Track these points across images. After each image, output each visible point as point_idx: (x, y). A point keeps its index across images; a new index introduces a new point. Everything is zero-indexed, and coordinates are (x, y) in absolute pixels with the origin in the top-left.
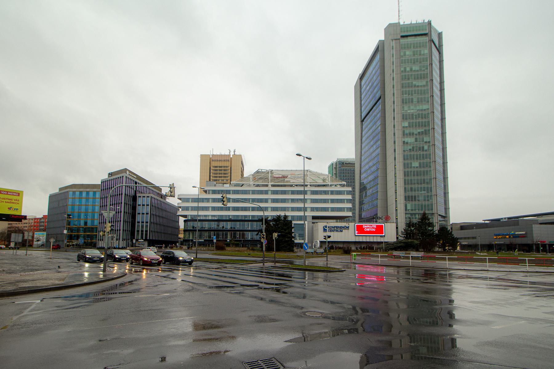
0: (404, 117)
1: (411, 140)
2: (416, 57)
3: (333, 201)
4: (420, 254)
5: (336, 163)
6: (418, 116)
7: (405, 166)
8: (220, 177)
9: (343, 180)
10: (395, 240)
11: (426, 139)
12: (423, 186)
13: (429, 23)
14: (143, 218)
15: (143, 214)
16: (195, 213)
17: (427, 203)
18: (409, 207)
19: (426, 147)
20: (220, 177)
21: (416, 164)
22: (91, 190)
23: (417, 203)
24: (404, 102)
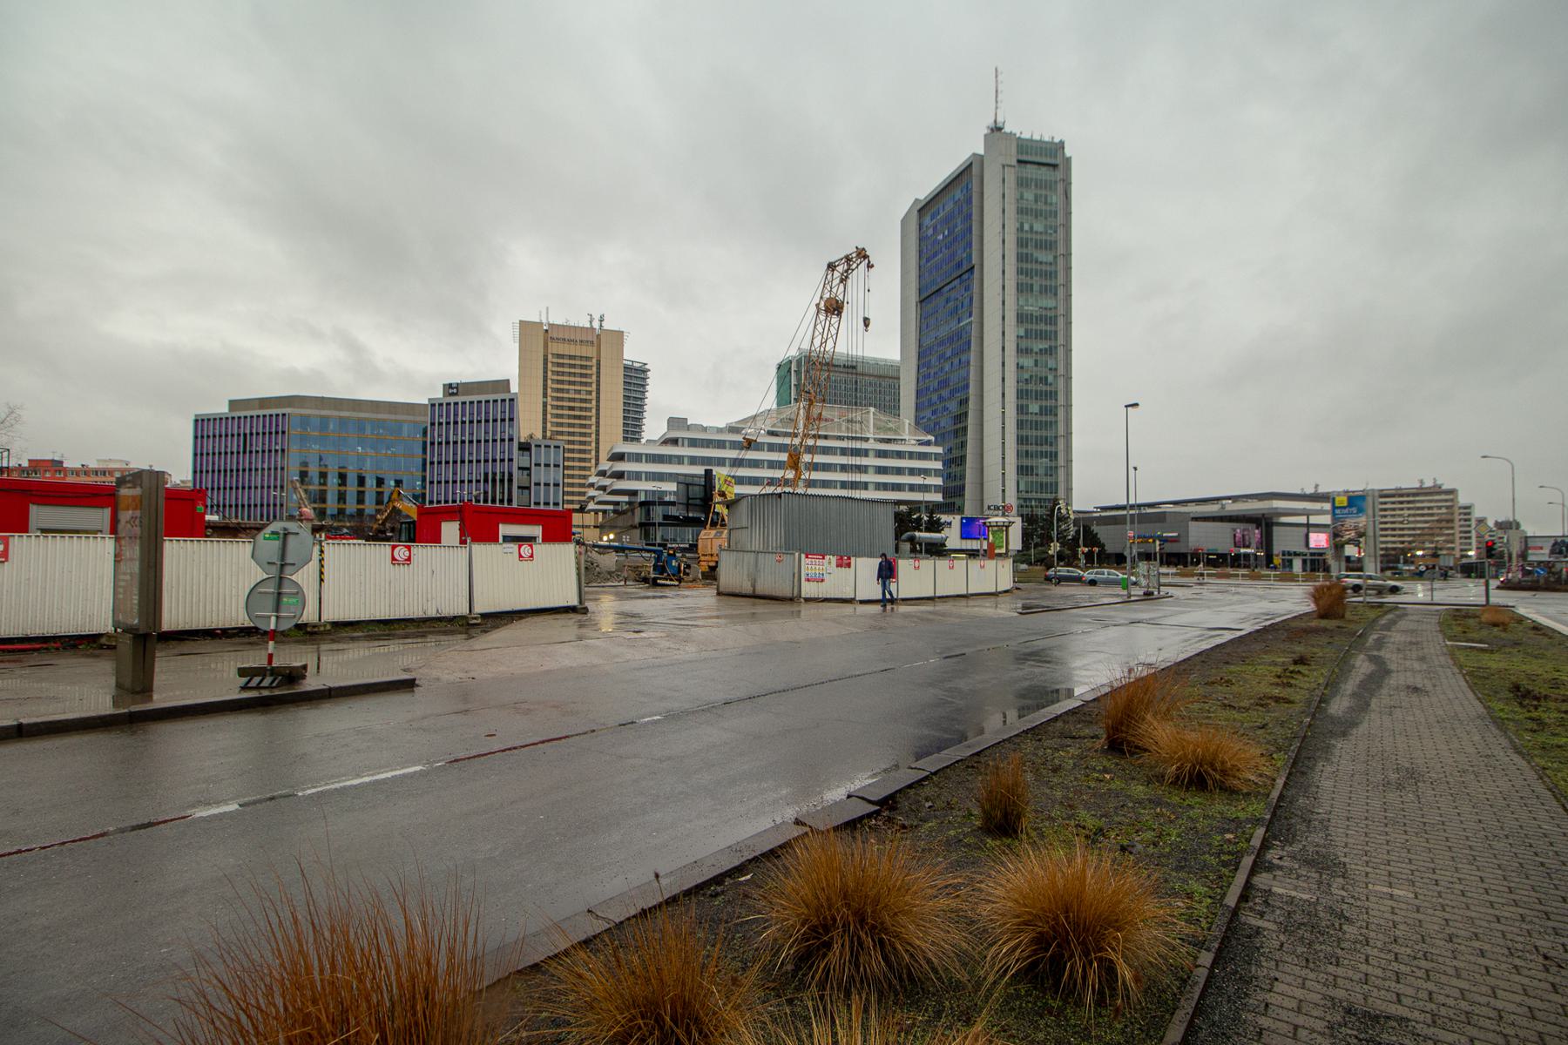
0: (1021, 318)
1: (1028, 362)
2: (1041, 206)
3: (912, 472)
4: (1173, 570)
5: (799, 362)
6: (1040, 319)
7: (1021, 409)
8: (570, 383)
9: (929, 432)
10: (191, 485)
11: (1051, 364)
12: (1044, 448)
13: (1061, 145)
14: (547, 493)
15: (547, 485)
16: (650, 486)
17: (1049, 479)
18: (1022, 487)
19: (1050, 379)
20: (570, 383)
21: (1034, 407)
22: (336, 413)
23: (1034, 479)
24: (1020, 289)
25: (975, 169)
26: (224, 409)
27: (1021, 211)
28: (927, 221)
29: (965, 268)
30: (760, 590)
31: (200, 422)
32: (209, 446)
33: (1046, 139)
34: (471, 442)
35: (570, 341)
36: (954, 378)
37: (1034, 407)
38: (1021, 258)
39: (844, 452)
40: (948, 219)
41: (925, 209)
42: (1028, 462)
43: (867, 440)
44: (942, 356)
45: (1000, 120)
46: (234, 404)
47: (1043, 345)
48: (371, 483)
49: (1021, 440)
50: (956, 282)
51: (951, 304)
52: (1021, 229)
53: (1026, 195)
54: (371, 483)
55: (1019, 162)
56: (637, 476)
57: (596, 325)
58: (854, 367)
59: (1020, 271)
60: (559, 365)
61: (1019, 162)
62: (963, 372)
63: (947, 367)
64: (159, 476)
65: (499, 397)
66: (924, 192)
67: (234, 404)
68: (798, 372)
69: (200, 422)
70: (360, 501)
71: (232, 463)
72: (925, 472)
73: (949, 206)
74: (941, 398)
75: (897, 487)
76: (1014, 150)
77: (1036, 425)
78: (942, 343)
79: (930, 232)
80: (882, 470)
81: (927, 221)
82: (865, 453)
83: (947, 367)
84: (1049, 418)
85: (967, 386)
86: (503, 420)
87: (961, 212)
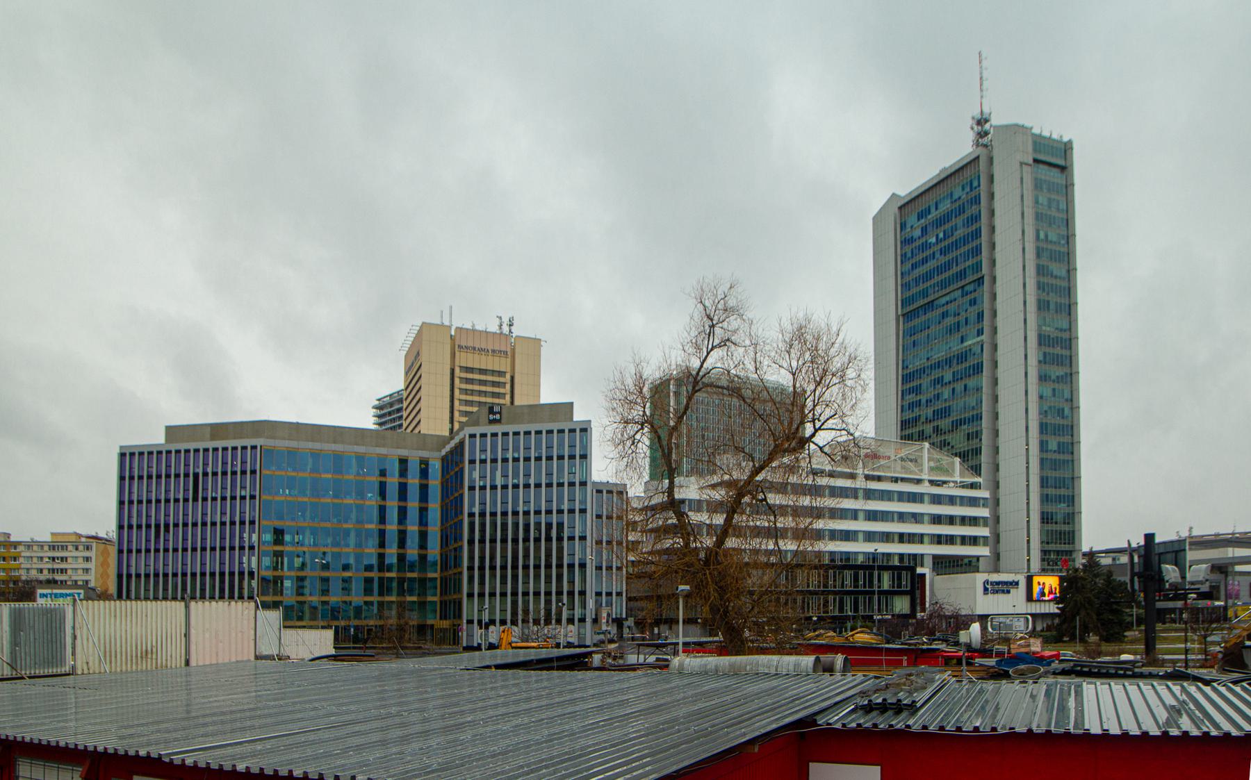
3: (964, 521)
7: (1043, 446)
12: (1062, 492)
16: (869, 548)
17: (1066, 528)
19: (1067, 411)
21: (1053, 445)
27: (1039, 217)
31: (126, 456)
33: (1055, 136)
34: (244, 472)
35: (481, 350)
36: (958, 404)
37: (1053, 445)
38: (1041, 270)
39: (902, 497)
42: (1050, 508)
43: (919, 481)
45: (986, 110)
49: (1044, 482)
51: (949, 321)
53: (1040, 200)
55: (1036, 161)
57: (506, 329)
59: (1040, 286)
60: (468, 381)
61: (1036, 161)
62: (972, 401)
63: (946, 393)
65: (555, 427)
67: (172, 432)
69: (126, 456)
71: (174, 513)
72: (974, 521)
74: (937, 430)
77: (1055, 465)
78: (938, 365)
79: (917, 233)
80: (937, 519)
81: (912, 220)
83: (946, 393)
85: (979, 417)
86: (572, 457)
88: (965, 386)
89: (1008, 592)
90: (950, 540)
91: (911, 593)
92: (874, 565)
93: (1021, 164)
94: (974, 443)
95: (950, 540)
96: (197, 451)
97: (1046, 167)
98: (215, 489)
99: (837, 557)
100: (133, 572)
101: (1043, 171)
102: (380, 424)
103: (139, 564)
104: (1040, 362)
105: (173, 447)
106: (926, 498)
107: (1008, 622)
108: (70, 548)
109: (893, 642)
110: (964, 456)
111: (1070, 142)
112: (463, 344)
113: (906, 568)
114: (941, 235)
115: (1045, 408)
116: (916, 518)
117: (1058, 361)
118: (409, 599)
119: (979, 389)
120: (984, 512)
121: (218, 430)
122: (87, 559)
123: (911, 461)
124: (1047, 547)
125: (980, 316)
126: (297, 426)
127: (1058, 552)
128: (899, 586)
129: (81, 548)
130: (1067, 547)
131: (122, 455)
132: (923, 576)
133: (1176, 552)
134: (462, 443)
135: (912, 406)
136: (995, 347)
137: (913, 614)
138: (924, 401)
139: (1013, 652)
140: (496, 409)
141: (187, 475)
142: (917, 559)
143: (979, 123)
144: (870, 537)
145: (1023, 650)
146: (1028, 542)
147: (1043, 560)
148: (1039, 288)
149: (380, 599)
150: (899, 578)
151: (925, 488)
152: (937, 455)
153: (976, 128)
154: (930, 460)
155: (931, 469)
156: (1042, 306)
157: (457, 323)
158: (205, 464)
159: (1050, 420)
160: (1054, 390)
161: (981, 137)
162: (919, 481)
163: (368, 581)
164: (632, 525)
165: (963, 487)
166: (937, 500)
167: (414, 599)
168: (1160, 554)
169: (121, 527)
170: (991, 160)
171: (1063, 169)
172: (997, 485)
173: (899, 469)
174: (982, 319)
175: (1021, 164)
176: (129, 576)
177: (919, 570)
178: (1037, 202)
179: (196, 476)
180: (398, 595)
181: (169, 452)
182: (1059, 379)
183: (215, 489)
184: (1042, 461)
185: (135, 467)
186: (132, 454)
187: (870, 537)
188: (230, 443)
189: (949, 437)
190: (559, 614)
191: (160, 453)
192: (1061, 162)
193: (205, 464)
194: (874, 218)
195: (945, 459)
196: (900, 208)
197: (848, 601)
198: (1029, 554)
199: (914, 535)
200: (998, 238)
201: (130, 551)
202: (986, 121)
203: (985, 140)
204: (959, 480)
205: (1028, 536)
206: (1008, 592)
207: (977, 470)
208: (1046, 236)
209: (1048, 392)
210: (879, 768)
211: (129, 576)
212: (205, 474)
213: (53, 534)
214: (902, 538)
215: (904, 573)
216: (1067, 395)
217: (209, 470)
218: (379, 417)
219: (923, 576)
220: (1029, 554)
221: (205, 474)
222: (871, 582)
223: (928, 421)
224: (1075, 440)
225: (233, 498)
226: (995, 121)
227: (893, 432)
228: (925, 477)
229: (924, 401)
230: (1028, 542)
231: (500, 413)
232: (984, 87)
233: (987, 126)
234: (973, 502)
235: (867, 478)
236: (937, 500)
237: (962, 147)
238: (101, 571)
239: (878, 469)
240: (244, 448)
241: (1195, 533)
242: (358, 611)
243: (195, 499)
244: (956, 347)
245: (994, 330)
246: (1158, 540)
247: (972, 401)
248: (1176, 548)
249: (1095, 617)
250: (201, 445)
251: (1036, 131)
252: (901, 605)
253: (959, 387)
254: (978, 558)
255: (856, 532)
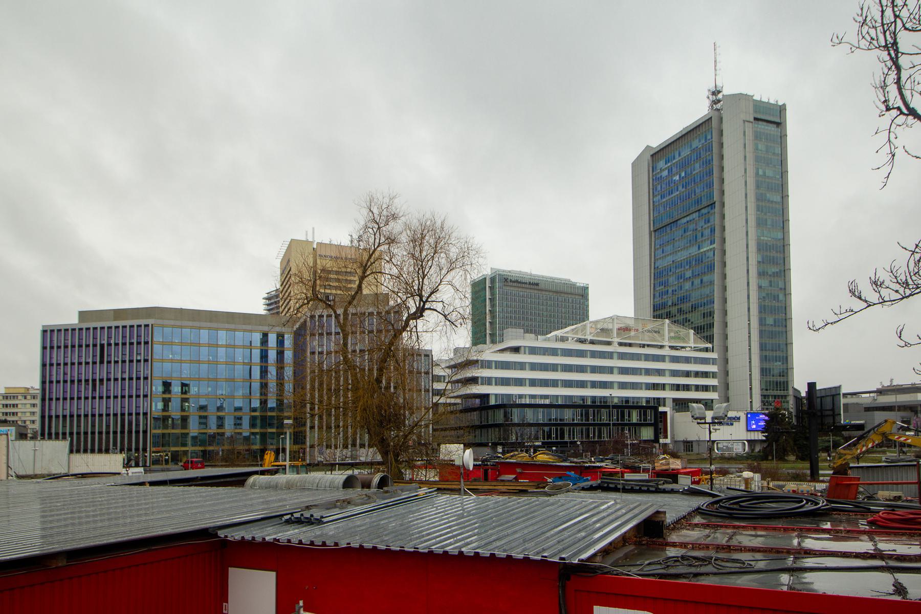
3: (697, 374)
7: (762, 322)
12: (778, 354)
17: (782, 379)
19: (781, 297)
21: (770, 320)
25: (714, 123)
26: (72, 320)
27: (757, 159)
28: (661, 164)
29: (705, 203)
30: (38, 472)
31: (48, 333)
32: (58, 356)
33: (772, 101)
38: (760, 198)
39: (648, 358)
40: (685, 164)
41: (658, 155)
43: (662, 347)
44: (681, 277)
45: (719, 84)
46: (83, 315)
47: (775, 269)
48: (176, 389)
49: (762, 347)
50: (695, 215)
52: (757, 174)
53: (760, 147)
54: (176, 389)
55: (756, 119)
56: (488, 381)
58: (537, 284)
59: (759, 208)
61: (756, 119)
62: (706, 291)
64: (799, 392)
66: (657, 140)
67: (83, 315)
68: (492, 288)
69: (48, 333)
70: (166, 402)
71: (86, 373)
72: (705, 375)
73: (686, 152)
74: (680, 311)
75: (582, 384)
76: (751, 110)
77: (772, 335)
79: (665, 173)
82: (610, 355)
84: (780, 329)
87: (699, 157)
88: (702, 281)
89: (732, 424)
90: (687, 388)
91: (655, 425)
92: (626, 406)
93: (744, 121)
94: (708, 320)
95: (687, 388)
96: (102, 328)
97: (765, 123)
98: (116, 355)
99: (598, 401)
100: (53, 414)
101: (762, 126)
102: (269, 310)
103: (58, 409)
104: (759, 262)
105: (84, 326)
106: (667, 359)
107: (730, 446)
108: (20, 397)
109: (564, 461)
110: (698, 330)
111: (784, 105)
112: (323, 253)
113: (650, 408)
114: (683, 174)
115: (764, 295)
116: (660, 372)
117: (773, 261)
118: (270, 430)
119: (712, 283)
120: (713, 368)
121: (119, 314)
122: (34, 405)
123: (655, 332)
124: (765, 393)
125: (713, 231)
126: (181, 311)
127: (775, 397)
128: (645, 420)
129: (29, 397)
130: (782, 393)
131: (44, 332)
132: (666, 413)
133: (833, 396)
134: (305, 321)
135: (662, 294)
136: (724, 252)
137: (656, 440)
138: (670, 291)
139: (657, 468)
140: (331, 298)
141: (95, 345)
142: (660, 401)
143: (714, 93)
144: (623, 386)
145: (664, 467)
146: (751, 389)
147: (762, 402)
148: (758, 210)
149: (262, 431)
150: (645, 414)
151: (666, 352)
152: (675, 328)
153: (711, 97)
154: (669, 331)
155: (671, 338)
156: (760, 223)
157: (318, 240)
158: (109, 338)
159: (767, 303)
160: (770, 282)
161: (716, 103)
162: (662, 347)
163: (253, 419)
164: (438, 379)
165: (697, 350)
166: (675, 359)
167: (274, 430)
168: (821, 397)
169: (43, 382)
170: (721, 120)
171: (778, 124)
172: (726, 349)
173: (646, 338)
174: (717, 234)
175: (744, 121)
176: (50, 417)
177: (661, 409)
178: (757, 149)
179: (102, 346)
180: (262, 427)
181: (81, 329)
182: (776, 275)
183: (116, 355)
184: (761, 333)
185: (53, 340)
186: (52, 331)
187: (623, 386)
188: (128, 323)
189: (689, 316)
190: (354, 441)
191: (73, 330)
192: (778, 120)
193: (109, 338)
194: (634, 165)
195: (683, 331)
196: (652, 156)
197: (605, 430)
198: (751, 397)
199: (626, 383)
200: (726, 175)
201: (51, 399)
202: (719, 92)
203: (719, 106)
204: (693, 345)
205: (751, 385)
206: (732, 424)
207: (710, 339)
208: (764, 173)
209: (765, 283)
210: (274, 574)
211: (50, 417)
212: (109, 345)
213: (6, 388)
214: (594, 384)
215: (649, 411)
216: (781, 285)
217: (112, 342)
218: (268, 305)
219: (666, 413)
220: (751, 397)
221: (109, 345)
222: (623, 416)
223: (674, 305)
224: (788, 317)
225: (131, 361)
226: (726, 91)
227: (648, 312)
228: (666, 343)
229: (670, 291)
230: (751, 389)
231: (334, 300)
232: (717, 68)
233: (720, 96)
234: (705, 361)
235: (621, 344)
236: (675, 359)
237: (700, 110)
238: (29, 413)
239: (629, 338)
240: (139, 326)
241: (895, 383)
242: (246, 439)
243: (102, 362)
244: (694, 251)
245: (724, 240)
246: (818, 388)
247: (706, 291)
248: (833, 392)
249: (792, 443)
250: (106, 324)
251: (757, 98)
252: (647, 434)
253: (697, 281)
254: (712, 400)
255: (612, 383)
